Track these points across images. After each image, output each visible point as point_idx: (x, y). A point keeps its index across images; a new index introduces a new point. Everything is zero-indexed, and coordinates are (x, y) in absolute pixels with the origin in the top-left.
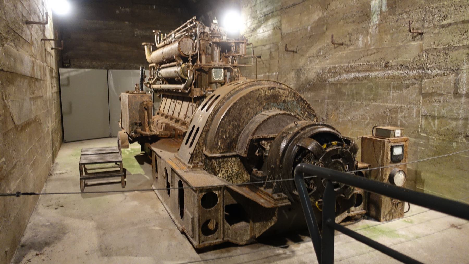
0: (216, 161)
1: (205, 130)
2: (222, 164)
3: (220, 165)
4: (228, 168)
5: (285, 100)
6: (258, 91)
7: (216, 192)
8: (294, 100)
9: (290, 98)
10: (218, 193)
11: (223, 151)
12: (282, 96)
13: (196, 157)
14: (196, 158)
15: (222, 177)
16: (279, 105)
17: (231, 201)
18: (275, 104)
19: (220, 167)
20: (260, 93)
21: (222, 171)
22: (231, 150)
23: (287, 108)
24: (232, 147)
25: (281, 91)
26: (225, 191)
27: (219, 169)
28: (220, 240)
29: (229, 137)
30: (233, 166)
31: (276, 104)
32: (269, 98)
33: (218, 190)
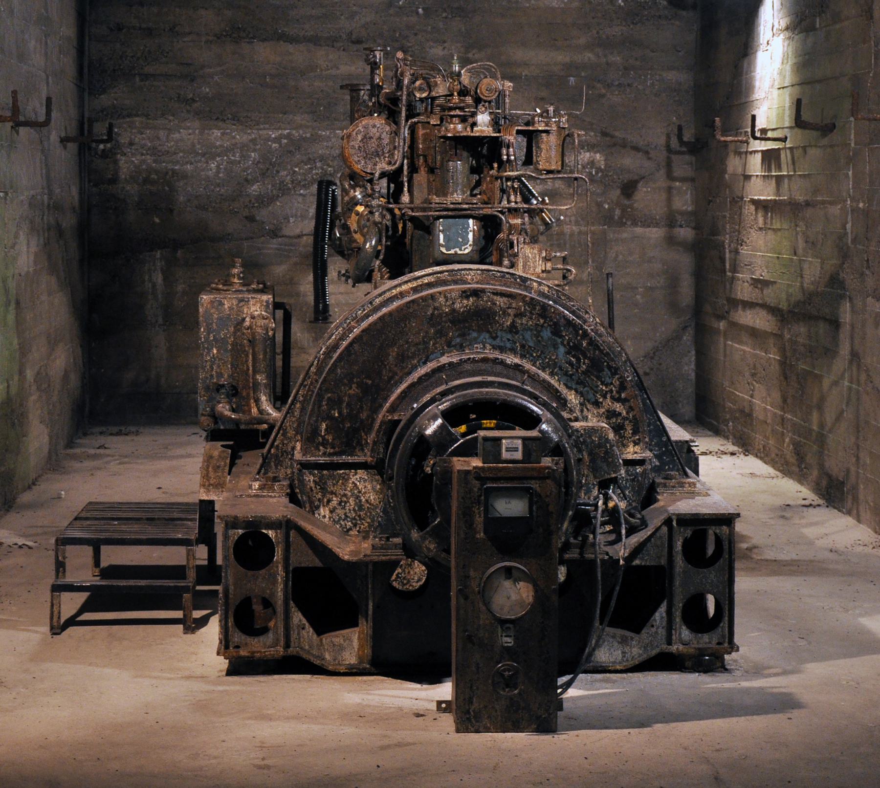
0: (314, 475)
1: (301, 399)
2: (330, 483)
4: (345, 495)
5: (513, 325)
6: (430, 301)
7: (271, 533)
8: (542, 326)
9: (531, 318)
10: (276, 536)
11: (332, 451)
12: (504, 312)
14: (276, 468)
15: (330, 518)
16: (495, 338)
17: (309, 560)
19: (324, 490)
20: (437, 304)
21: (329, 501)
22: (355, 448)
23: (523, 346)
24: (359, 443)
25: (500, 301)
26: (292, 533)
27: (319, 496)
28: (280, 650)
30: (360, 492)
31: (487, 335)
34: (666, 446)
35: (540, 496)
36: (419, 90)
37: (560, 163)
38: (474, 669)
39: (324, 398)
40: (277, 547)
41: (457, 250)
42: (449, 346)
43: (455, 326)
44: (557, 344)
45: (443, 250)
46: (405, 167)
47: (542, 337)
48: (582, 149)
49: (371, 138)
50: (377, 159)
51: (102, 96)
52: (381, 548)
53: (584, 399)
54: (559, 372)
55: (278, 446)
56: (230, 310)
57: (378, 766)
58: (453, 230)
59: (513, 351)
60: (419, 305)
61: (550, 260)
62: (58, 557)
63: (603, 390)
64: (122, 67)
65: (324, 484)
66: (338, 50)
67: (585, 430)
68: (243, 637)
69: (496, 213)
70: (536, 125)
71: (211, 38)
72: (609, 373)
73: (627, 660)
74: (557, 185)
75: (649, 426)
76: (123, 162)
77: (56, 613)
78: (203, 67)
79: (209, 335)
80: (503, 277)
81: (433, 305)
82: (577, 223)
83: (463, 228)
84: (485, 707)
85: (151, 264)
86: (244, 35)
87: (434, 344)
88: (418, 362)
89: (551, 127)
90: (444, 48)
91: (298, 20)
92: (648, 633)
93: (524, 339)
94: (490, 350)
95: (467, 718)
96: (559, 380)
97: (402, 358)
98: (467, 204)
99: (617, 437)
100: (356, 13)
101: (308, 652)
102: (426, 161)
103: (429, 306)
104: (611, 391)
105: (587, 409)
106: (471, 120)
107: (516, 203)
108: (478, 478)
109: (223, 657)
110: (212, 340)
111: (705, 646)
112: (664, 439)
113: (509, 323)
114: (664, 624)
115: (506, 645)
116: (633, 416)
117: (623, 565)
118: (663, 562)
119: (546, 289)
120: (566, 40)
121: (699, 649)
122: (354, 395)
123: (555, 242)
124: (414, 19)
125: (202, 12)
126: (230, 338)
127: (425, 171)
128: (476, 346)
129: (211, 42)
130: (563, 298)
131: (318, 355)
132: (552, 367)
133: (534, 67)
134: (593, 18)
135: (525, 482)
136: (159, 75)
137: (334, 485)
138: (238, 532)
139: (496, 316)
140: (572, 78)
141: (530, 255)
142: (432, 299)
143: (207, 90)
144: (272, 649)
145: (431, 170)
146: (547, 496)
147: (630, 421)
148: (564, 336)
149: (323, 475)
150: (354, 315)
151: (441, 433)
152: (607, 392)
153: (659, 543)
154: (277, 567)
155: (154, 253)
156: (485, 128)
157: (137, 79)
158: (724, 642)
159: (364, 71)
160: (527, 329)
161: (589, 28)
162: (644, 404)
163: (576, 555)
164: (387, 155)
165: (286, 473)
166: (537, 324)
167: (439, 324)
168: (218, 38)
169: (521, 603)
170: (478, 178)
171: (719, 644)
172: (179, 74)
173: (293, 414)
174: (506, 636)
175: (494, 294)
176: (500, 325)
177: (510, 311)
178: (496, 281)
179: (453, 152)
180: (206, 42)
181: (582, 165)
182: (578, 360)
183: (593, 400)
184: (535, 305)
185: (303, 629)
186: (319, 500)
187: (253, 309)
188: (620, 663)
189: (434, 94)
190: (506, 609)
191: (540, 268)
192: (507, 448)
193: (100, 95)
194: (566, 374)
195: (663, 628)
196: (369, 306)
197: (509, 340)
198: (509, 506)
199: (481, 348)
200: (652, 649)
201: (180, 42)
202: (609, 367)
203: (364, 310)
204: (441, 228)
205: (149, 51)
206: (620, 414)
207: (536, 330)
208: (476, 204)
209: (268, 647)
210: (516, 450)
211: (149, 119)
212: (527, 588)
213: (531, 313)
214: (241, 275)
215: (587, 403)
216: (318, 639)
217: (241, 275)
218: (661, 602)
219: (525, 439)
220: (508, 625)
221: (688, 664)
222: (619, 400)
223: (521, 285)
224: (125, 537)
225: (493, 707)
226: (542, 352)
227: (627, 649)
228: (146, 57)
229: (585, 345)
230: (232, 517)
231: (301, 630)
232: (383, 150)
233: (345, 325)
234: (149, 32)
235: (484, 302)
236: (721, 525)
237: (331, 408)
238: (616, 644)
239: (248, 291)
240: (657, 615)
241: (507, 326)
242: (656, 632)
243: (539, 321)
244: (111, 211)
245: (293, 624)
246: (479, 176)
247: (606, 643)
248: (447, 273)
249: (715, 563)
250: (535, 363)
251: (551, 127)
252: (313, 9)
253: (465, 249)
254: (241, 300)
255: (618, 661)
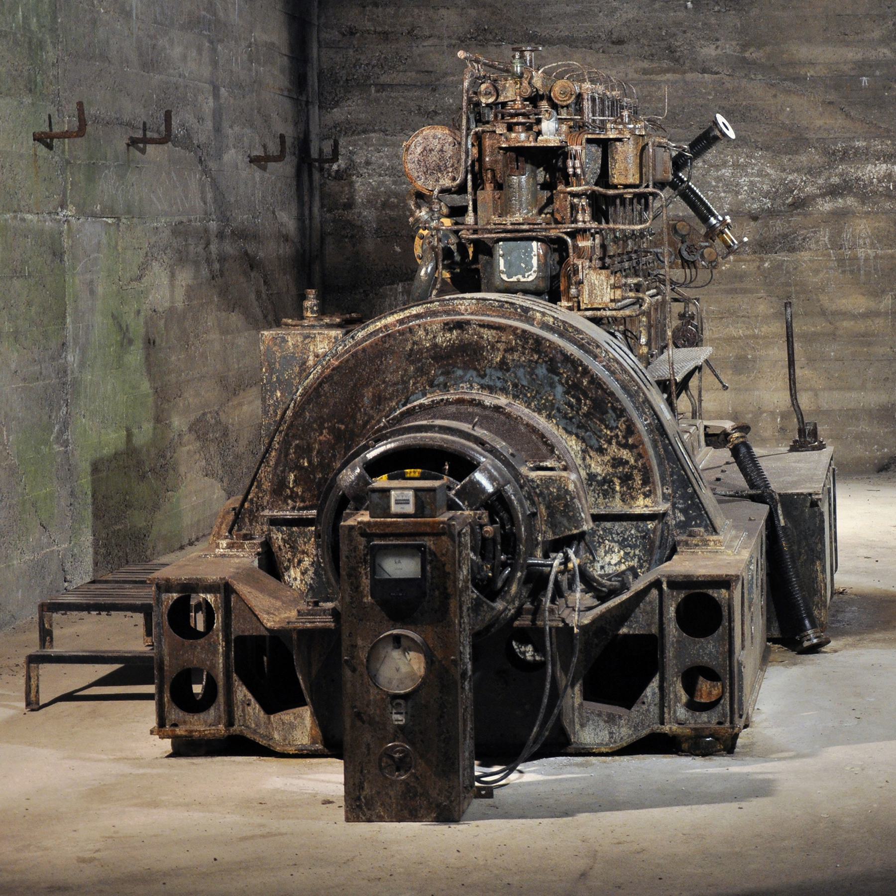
1: (277, 446)
2: (300, 541)
3: (293, 542)
5: (503, 362)
6: (408, 335)
8: (536, 362)
9: (524, 354)
10: (216, 601)
11: (302, 505)
13: (251, 522)
14: (251, 525)
15: (301, 580)
16: (483, 376)
18: (471, 374)
19: (294, 548)
20: (416, 338)
21: (300, 562)
23: (515, 386)
25: (488, 334)
27: (289, 555)
29: (321, 464)
31: (474, 373)
32: (449, 356)
33: (214, 593)
34: (692, 498)
35: (435, 554)
36: (486, 94)
37: (637, 176)
38: (365, 750)
39: (291, 445)
40: (217, 613)
41: (520, 277)
42: (431, 386)
43: (438, 363)
44: (553, 383)
45: (504, 277)
46: (470, 184)
47: (536, 375)
48: (878, 160)
49: (431, 150)
50: (439, 175)
51: (335, 110)
52: (308, 614)
53: (587, 446)
54: (557, 414)
55: (252, 500)
56: (294, 348)
57: (215, 859)
58: (515, 254)
59: (504, 390)
60: (395, 339)
61: (619, 287)
62: (44, 625)
63: (608, 435)
64: (355, 77)
65: (293, 542)
66: (597, 52)
67: (541, 480)
68: (181, 714)
69: (561, 235)
70: (609, 133)
71: (454, 42)
72: (614, 415)
73: (615, 742)
74: (849, 203)
75: (671, 476)
76: (359, 184)
77: (33, 687)
78: (445, 74)
79: (271, 376)
80: (502, 306)
81: (412, 339)
82: (873, 246)
83: (526, 251)
84: (378, 793)
85: (393, 298)
86: (490, 37)
87: (414, 384)
88: (397, 404)
89: (623, 134)
90: (717, 47)
91: (551, 19)
92: (638, 711)
93: (516, 377)
94: (478, 390)
95: (358, 806)
96: (557, 424)
97: (379, 400)
98: (529, 224)
99: (625, 489)
100: (616, 9)
101: (255, 732)
102: (494, 176)
103: (407, 340)
104: (617, 436)
105: (590, 457)
106: (535, 128)
107: (584, 222)
108: (363, 534)
109: (158, 737)
110: (276, 382)
111: (704, 726)
112: (690, 490)
113: (498, 359)
114: (657, 700)
115: (396, 723)
116: (642, 464)
117: (577, 633)
118: (654, 630)
119: (551, 320)
120: (857, 34)
121: (695, 729)
122: (325, 441)
123: (848, 268)
124: (681, 14)
125: (443, 12)
126: (295, 379)
127: (491, 187)
128: (461, 385)
129: (454, 46)
130: (570, 330)
131: (295, 397)
132: (549, 409)
133: (821, 66)
134: (889, 8)
135: (417, 538)
136: (396, 85)
137: (305, 543)
138: (172, 597)
139: (484, 352)
140: (864, 78)
141: (596, 282)
142: (411, 333)
143: (451, 101)
144: (214, 728)
145: (499, 187)
146: (443, 555)
147: (639, 471)
148: (562, 374)
149: (293, 532)
150: (334, 352)
151: (357, 484)
152: (611, 437)
153: (648, 608)
154: (218, 635)
155: (396, 286)
156: (552, 137)
157: (373, 89)
158: (725, 721)
159: (626, 76)
160: (520, 366)
161: (884, 19)
162: (666, 450)
163: (527, 623)
164: (450, 170)
165: (262, 530)
166: (530, 361)
167: (419, 360)
168: (462, 41)
169: (411, 675)
170: (549, 194)
171: (720, 723)
172: (419, 84)
173: (268, 463)
174: (395, 713)
175: (480, 326)
176: (489, 361)
177: (499, 345)
178: (493, 311)
179: (514, 165)
180: (449, 46)
181: (877, 178)
182: (579, 400)
183: (597, 446)
184: (527, 338)
185: (249, 705)
186: (289, 560)
187: (320, 346)
188: (607, 744)
189: (501, 99)
190: (395, 683)
191: (608, 297)
192: (396, 500)
193: (332, 108)
194: (565, 416)
195: (655, 705)
196: (351, 340)
197: (499, 378)
198: (399, 566)
199: (467, 388)
200: (644, 729)
201: (420, 47)
202: (614, 409)
203: (345, 345)
204: (501, 252)
205: (385, 57)
206: (627, 462)
207: (530, 367)
208: (541, 224)
209: (210, 725)
210: (407, 502)
211: (386, 135)
212: (419, 659)
213: (523, 347)
214: (315, 308)
215: (590, 450)
216: (266, 716)
217: (315, 308)
218: (653, 676)
219: (417, 490)
220: (398, 701)
221: (685, 746)
222: (625, 446)
223: (521, 316)
224: (117, 602)
225: (387, 794)
226: (537, 392)
227: (615, 729)
228: (382, 65)
229: (585, 383)
230: (163, 579)
231: (246, 706)
232: (445, 163)
233: (324, 363)
234: (385, 36)
235: (469, 335)
236: (720, 588)
237: (299, 457)
238: (602, 724)
239: (321, 326)
240: (649, 691)
241: (497, 363)
242: (648, 710)
243: (532, 356)
244: (346, 240)
245: (237, 699)
246: (552, 191)
247: (591, 722)
248: (437, 303)
249: (714, 631)
250: (530, 404)
251: (623, 134)
252: (568, 5)
253: (528, 276)
254: (307, 337)
255: (605, 743)
